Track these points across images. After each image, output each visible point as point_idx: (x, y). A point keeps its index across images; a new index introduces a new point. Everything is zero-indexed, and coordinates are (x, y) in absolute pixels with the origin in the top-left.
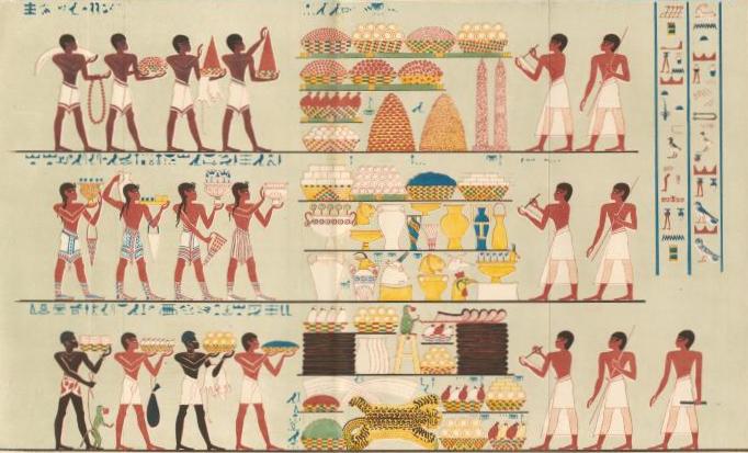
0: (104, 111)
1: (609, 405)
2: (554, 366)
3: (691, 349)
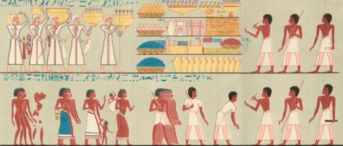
0: (60, 30)
1: (289, 51)
2: (262, 32)
3: (330, 24)
